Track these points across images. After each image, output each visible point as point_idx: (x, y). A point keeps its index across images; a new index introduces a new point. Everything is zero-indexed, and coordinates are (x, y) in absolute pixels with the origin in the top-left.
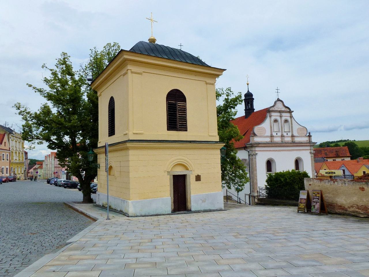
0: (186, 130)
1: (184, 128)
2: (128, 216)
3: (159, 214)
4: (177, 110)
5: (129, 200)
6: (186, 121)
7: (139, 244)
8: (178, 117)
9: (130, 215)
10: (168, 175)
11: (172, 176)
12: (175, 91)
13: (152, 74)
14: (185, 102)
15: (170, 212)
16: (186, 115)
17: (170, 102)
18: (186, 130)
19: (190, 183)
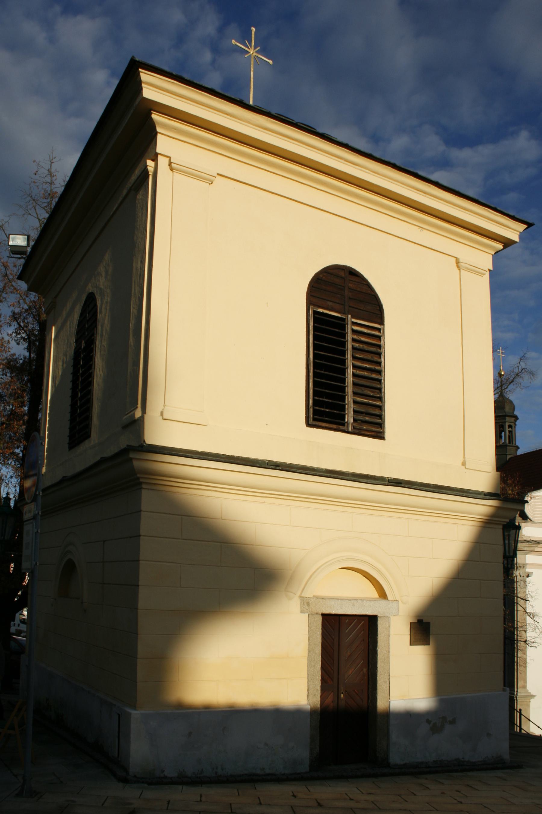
0: (382, 438)
1: (371, 424)
2: (125, 780)
3: (259, 772)
4: (350, 323)
5: (134, 707)
6: (381, 399)
7: (203, 799)
8: (350, 323)
9: (455, 259)
10: (302, 612)
11: (319, 619)
12: (342, 274)
13: (209, 86)
14: (382, 322)
15: (304, 768)
16: (380, 372)
17: (320, 310)
18: (380, 435)
19: (389, 652)
